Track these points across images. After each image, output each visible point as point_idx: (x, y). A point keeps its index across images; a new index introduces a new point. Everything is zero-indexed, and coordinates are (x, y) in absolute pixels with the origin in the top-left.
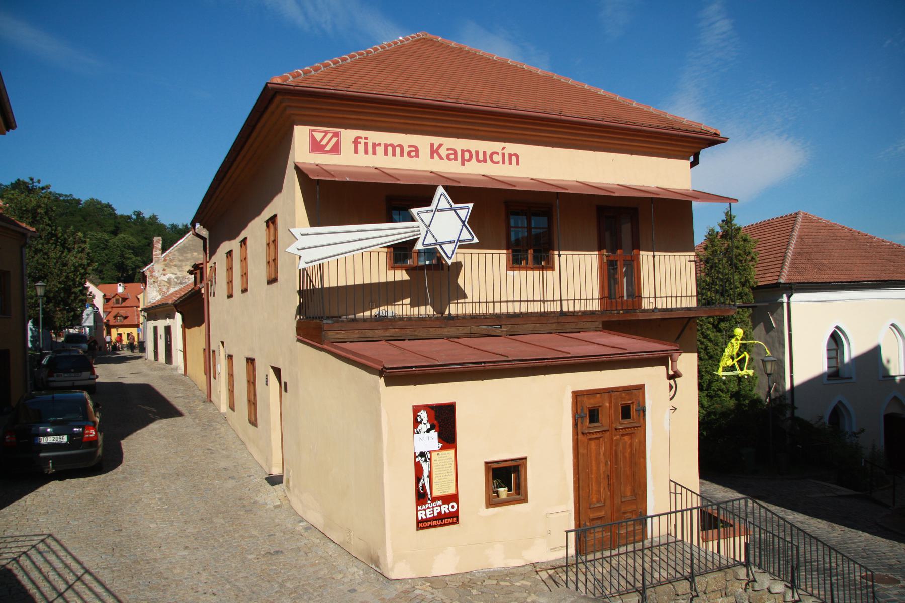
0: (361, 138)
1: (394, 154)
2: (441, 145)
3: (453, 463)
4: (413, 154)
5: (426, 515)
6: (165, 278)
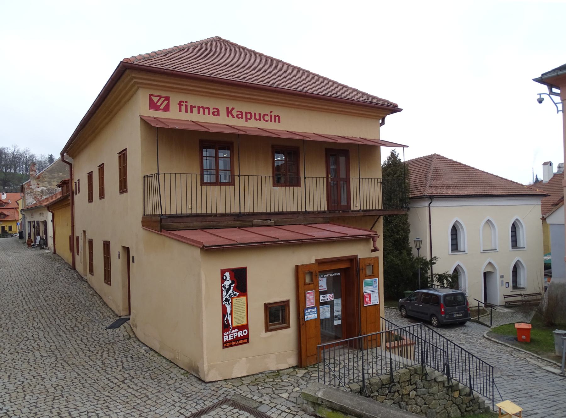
0: (183, 102)
1: (204, 113)
2: (233, 109)
3: (245, 305)
4: (216, 113)
5: (228, 338)
6: (39, 190)
